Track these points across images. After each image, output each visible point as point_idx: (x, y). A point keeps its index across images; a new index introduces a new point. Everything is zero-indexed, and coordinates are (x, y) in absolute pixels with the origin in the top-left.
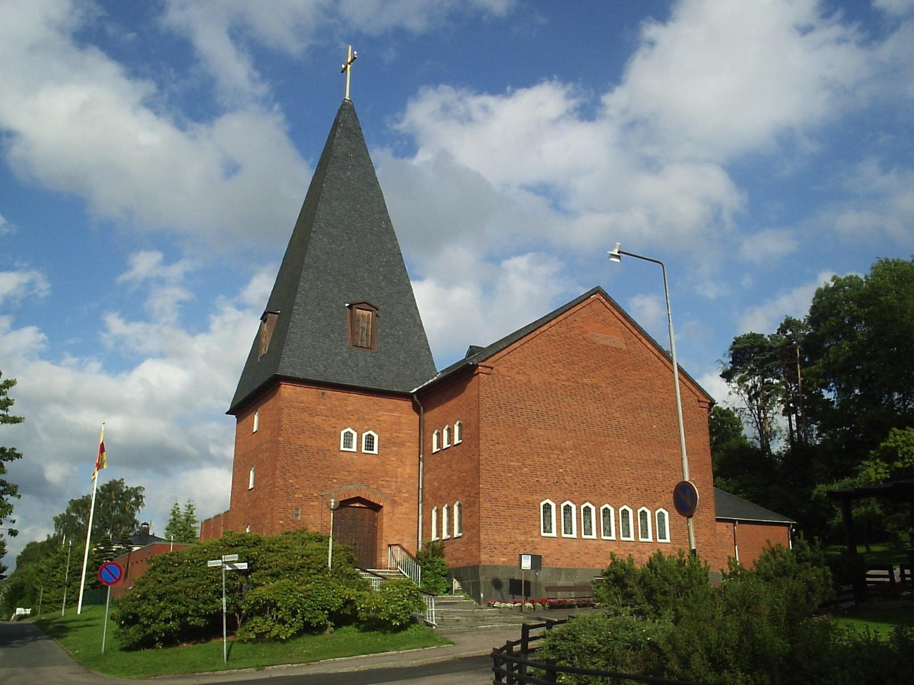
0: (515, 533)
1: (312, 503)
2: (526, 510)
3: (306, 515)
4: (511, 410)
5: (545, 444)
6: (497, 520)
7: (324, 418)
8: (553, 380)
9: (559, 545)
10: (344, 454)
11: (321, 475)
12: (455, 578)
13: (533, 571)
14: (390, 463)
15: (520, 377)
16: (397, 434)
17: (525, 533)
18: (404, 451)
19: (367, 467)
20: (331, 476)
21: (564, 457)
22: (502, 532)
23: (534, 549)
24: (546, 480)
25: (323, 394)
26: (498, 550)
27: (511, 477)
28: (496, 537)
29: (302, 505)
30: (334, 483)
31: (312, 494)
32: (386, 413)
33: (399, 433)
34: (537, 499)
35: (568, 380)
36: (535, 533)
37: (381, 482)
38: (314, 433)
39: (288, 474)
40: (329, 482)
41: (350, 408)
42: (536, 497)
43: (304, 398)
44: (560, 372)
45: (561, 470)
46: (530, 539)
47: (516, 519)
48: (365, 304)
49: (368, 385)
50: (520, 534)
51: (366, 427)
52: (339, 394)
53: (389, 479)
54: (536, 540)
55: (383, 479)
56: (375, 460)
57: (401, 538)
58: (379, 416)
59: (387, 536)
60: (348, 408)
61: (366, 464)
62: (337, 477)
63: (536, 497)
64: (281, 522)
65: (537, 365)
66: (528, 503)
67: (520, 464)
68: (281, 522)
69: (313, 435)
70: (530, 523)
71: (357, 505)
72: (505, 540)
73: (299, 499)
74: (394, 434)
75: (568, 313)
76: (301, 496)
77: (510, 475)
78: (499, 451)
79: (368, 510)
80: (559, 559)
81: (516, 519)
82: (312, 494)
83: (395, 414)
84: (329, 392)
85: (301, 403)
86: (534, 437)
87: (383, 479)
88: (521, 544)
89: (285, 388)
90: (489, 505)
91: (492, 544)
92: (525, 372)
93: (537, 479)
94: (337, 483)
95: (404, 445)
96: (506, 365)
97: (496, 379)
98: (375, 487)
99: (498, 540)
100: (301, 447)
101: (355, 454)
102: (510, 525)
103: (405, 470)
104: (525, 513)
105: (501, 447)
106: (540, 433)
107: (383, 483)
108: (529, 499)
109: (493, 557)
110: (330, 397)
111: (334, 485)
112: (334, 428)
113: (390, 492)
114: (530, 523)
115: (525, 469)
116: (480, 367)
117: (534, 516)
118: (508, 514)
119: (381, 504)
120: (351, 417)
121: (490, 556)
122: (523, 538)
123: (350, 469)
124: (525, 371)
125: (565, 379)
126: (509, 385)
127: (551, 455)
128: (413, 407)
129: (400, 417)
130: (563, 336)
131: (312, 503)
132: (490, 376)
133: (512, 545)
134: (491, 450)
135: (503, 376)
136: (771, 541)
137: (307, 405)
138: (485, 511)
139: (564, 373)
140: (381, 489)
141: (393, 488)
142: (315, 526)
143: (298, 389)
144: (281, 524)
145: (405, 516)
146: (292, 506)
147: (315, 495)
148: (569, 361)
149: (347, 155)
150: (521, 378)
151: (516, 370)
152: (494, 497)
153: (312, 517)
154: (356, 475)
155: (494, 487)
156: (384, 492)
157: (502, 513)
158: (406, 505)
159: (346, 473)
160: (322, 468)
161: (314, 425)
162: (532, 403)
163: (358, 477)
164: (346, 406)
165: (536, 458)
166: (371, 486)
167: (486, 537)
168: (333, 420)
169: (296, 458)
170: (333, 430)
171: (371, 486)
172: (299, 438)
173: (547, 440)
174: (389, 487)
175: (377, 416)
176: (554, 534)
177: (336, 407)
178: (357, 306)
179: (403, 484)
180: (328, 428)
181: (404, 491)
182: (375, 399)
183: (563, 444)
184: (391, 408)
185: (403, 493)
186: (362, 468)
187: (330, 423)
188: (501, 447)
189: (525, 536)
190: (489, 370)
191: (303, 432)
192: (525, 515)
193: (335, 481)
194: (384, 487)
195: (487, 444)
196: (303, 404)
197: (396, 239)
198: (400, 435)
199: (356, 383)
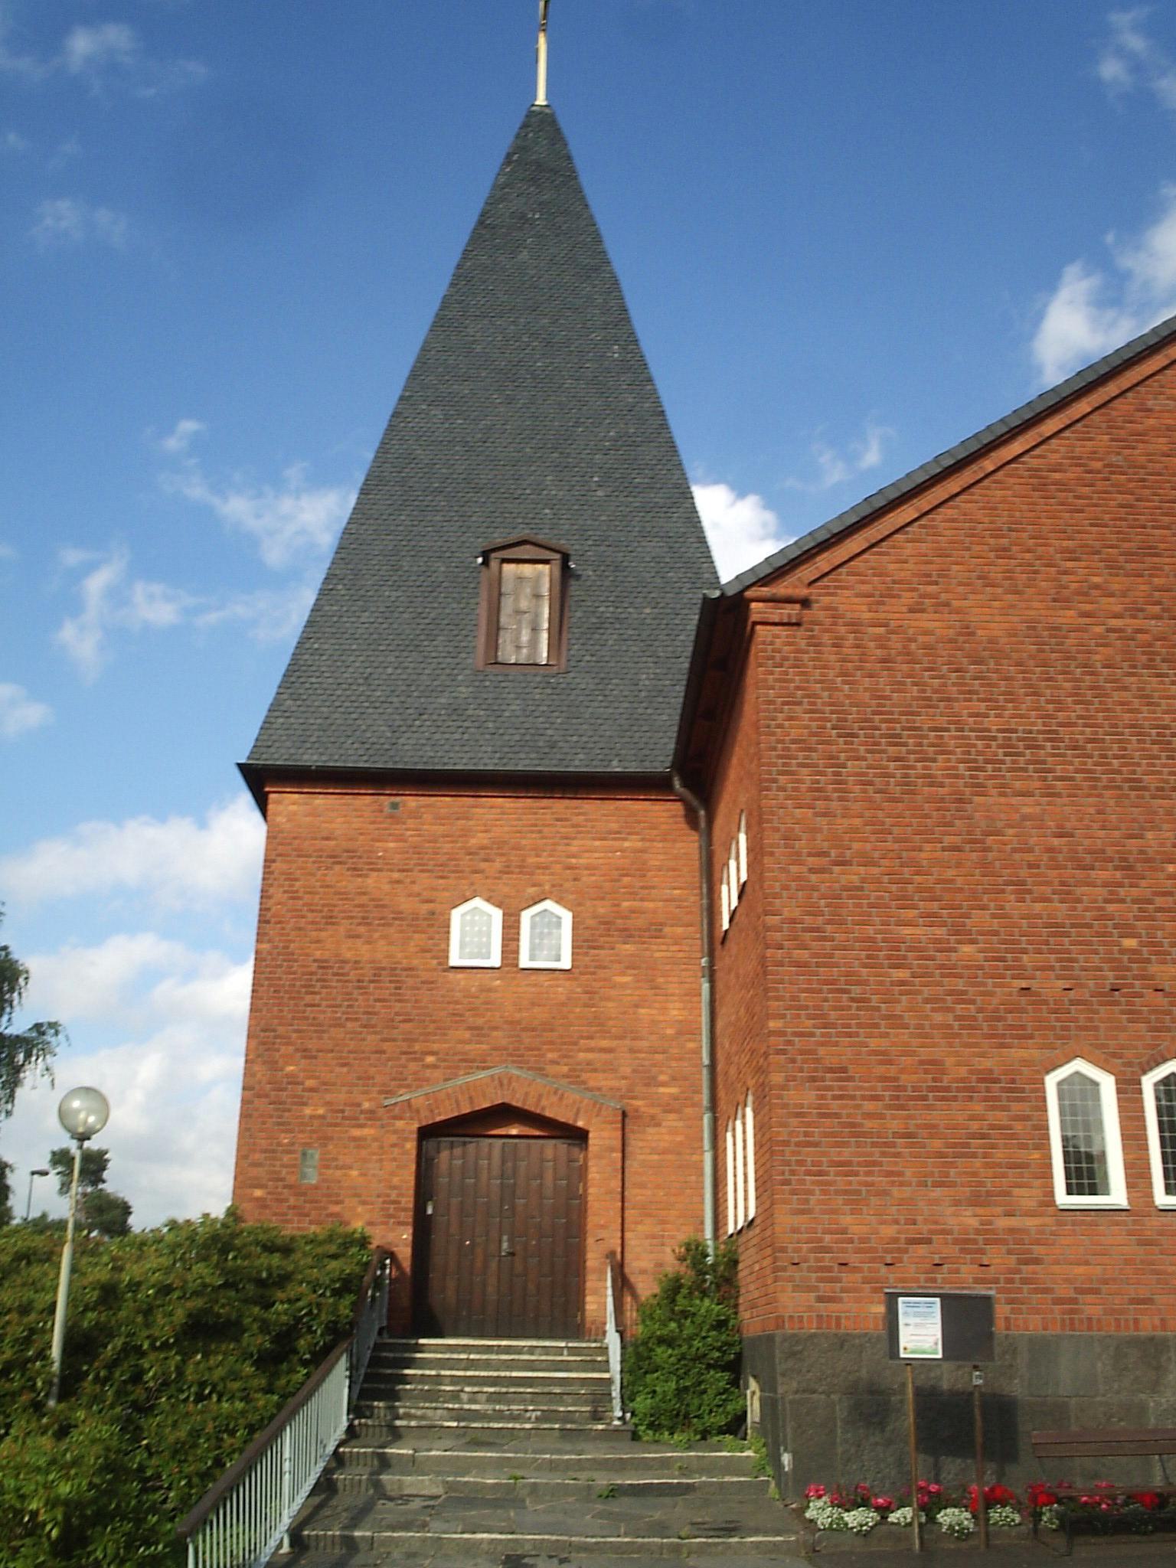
0: (932, 1202)
1: (356, 1132)
2: (978, 1108)
3: (337, 1168)
4: (894, 739)
5: (1050, 850)
6: (847, 1153)
7: (396, 875)
8: (1067, 617)
9: (1140, 1243)
10: (460, 976)
11: (386, 1046)
12: (755, 1377)
13: (947, 1366)
14: (613, 993)
15: (927, 621)
16: (637, 904)
17: (977, 1200)
18: (659, 952)
19: (536, 1010)
20: (417, 1047)
21: (1143, 889)
22: (873, 1200)
23: (1021, 1262)
24: (1062, 984)
25: (395, 806)
26: (856, 1270)
27: (902, 983)
28: (847, 1220)
29: (325, 1140)
30: (428, 1066)
31: (359, 1105)
32: (597, 843)
33: (642, 900)
34: (1025, 1062)
35: (1135, 611)
36: (1027, 1198)
37: (582, 1055)
38: (365, 921)
39: (283, 1049)
40: (413, 1066)
41: (478, 840)
42: (1023, 1053)
43: (339, 826)
44: (1097, 587)
45: (1130, 943)
46: (1003, 1223)
47: (937, 1144)
48: (528, 547)
49: (524, 763)
50: (957, 1203)
51: (532, 890)
52: (445, 804)
53: (614, 1043)
54: (1030, 1223)
55: (592, 1043)
56: (562, 990)
57: (657, 1229)
58: (574, 856)
59: (603, 1227)
60: (473, 841)
61: (533, 1004)
62: (435, 1047)
63: (1023, 1053)
64: (258, 1193)
65: (996, 574)
66: (987, 1077)
67: (941, 932)
68: (258, 1193)
69: (362, 929)
70: (999, 1155)
71: (514, 1132)
72: (889, 1231)
73: (316, 1122)
74: (625, 904)
75: (1112, 389)
76: (321, 1111)
77: (902, 974)
78: (845, 889)
79: (553, 1142)
80: (1148, 1301)
81: (937, 1144)
82: (359, 1105)
83: (626, 844)
84: (412, 802)
85: (327, 839)
86: (999, 824)
87: (592, 1043)
88: (965, 1243)
89: (279, 802)
90: (808, 1097)
91: (828, 1250)
92: (947, 604)
93: (1024, 984)
94: (434, 1067)
95: (658, 934)
96: (866, 588)
97: (826, 638)
98: (565, 1069)
99: (856, 1230)
100: (323, 964)
101: (496, 973)
102: (908, 1172)
103: (664, 1010)
104: (972, 1118)
105: (853, 875)
106: (1026, 810)
107: (590, 1056)
108: (988, 1063)
109: (839, 1300)
110: (415, 815)
111: (428, 1073)
112: (427, 901)
113: (615, 1083)
114: (999, 1155)
115: (967, 949)
116: (753, 605)
117: (1018, 1127)
118: (895, 1125)
119: (580, 1124)
120: (483, 865)
121: (820, 1299)
122: (970, 1219)
123: (480, 1021)
124: (944, 597)
125: (1118, 608)
126: (879, 652)
127: (1079, 890)
128: (686, 816)
129: (643, 851)
130: (1098, 465)
131: (356, 1132)
132: (800, 632)
133: (922, 1250)
134: (814, 888)
135: (855, 625)
136: (49, 1085)
137: (345, 845)
138: (794, 1121)
139: (1115, 587)
140: (584, 1076)
141: (627, 1070)
142: (364, 1203)
143: (319, 801)
144: (258, 1199)
145: (670, 1157)
146: (293, 1144)
147: (366, 1105)
148: (1132, 546)
149: (523, 216)
150: (931, 625)
151: (908, 599)
152: (831, 1061)
153: (354, 1173)
154: (500, 1037)
155: (833, 1026)
156: (592, 1084)
157: (869, 1125)
158: (671, 1121)
159: (467, 1035)
160: (390, 1024)
161: (364, 899)
162: (983, 707)
163: (504, 1042)
164: (466, 833)
165: (1011, 904)
166: (551, 1069)
167: (796, 1220)
168: (424, 880)
169: (308, 999)
170: (426, 907)
171: (551, 1069)
172: (318, 942)
173: (1060, 836)
174: (610, 1068)
175: (569, 857)
176: (1117, 1195)
177: (435, 842)
178: (507, 554)
179: (659, 1057)
180: (406, 904)
181: (662, 1078)
182: (560, 806)
183: (1132, 844)
184: (614, 826)
185: (664, 1084)
186: (518, 1016)
187: (416, 888)
188: (853, 875)
189: (980, 1210)
190: (792, 611)
191: (330, 921)
192: (974, 1126)
193: (430, 1059)
194: (595, 1070)
195: (794, 869)
196: (333, 843)
197: (650, 380)
198: (646, 904)
199: (489, 763)
